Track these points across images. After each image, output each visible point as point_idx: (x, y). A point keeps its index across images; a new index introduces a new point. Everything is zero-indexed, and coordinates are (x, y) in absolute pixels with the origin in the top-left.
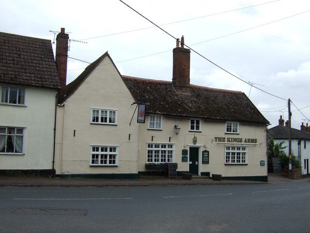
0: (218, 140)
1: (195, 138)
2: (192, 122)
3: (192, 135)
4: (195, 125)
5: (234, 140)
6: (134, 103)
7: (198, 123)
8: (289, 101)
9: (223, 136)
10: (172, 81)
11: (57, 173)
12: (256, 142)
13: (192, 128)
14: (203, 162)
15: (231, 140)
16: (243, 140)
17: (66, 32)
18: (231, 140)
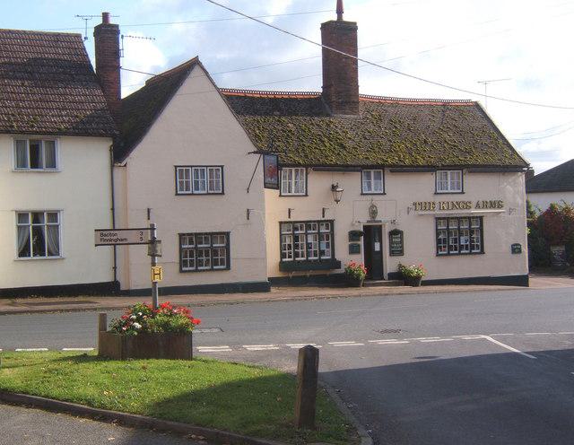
1: (373, 206)
2: (19, 144)
3: (366, 201)
6: (254, 152)
9: (429, 197)
10: (321, 91)
11: (123, 287)
12: (500, 206)
14: (392, 253)
17: (112, 21)
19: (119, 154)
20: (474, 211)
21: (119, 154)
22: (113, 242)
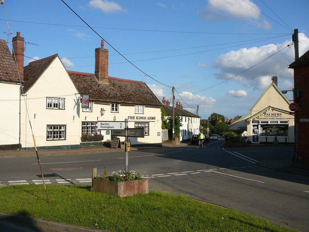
0: (130, 118)
2: (113, 106)
4: (115, 107)
5: (142, 118)
7: (116, 106)
8: (173, 88)
13: (113, 109)
15: (138, 118)
16: (147, 118)
17: (106, 46)
18: (138, 118)
19: (24, 90)
20: (147, 120)
21: (24, 90)
22: (107, 129)
